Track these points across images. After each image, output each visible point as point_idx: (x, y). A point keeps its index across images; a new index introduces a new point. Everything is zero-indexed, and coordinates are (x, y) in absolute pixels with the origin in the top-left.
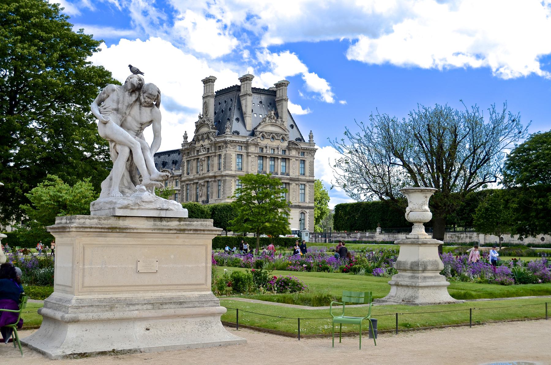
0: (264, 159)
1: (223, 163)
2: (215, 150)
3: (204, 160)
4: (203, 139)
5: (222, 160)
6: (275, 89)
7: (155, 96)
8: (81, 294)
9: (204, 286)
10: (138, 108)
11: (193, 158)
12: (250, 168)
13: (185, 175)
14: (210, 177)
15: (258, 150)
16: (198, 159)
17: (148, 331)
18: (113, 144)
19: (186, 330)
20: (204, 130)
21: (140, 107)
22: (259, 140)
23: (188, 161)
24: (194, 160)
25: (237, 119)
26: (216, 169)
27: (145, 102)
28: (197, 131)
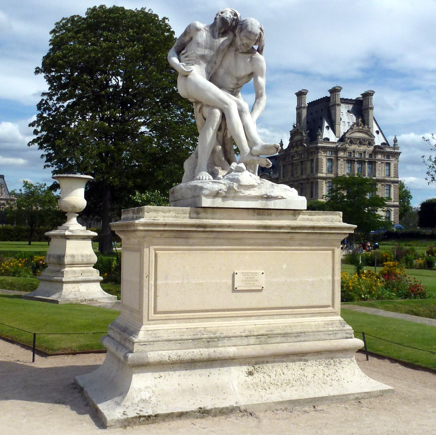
0: (353, 162)
1: (315, 166)
2: (308, 155)
3: (298, 165)
4: (297, 146)
5: (314, 164)
6: (362, 99)
7: (256, 35)
8: (152, 322)
9: (330, 309)
10: (233, 55)
11: (288, 163)
12: (339, 171)
13: (282, 178)
14: (304, 179)
15: (346, 155)
16: (293, 164)
17: (251, 377)
18: (199, 106)
19: (306, 374)
20: (297, 138)
21: (236, 55)
22: (347, 146)
23: (284, 166)
24: (289, 164)
25: (327, 127)
26: (309, 172)
27: (243, 45)
28: (291, 139)
